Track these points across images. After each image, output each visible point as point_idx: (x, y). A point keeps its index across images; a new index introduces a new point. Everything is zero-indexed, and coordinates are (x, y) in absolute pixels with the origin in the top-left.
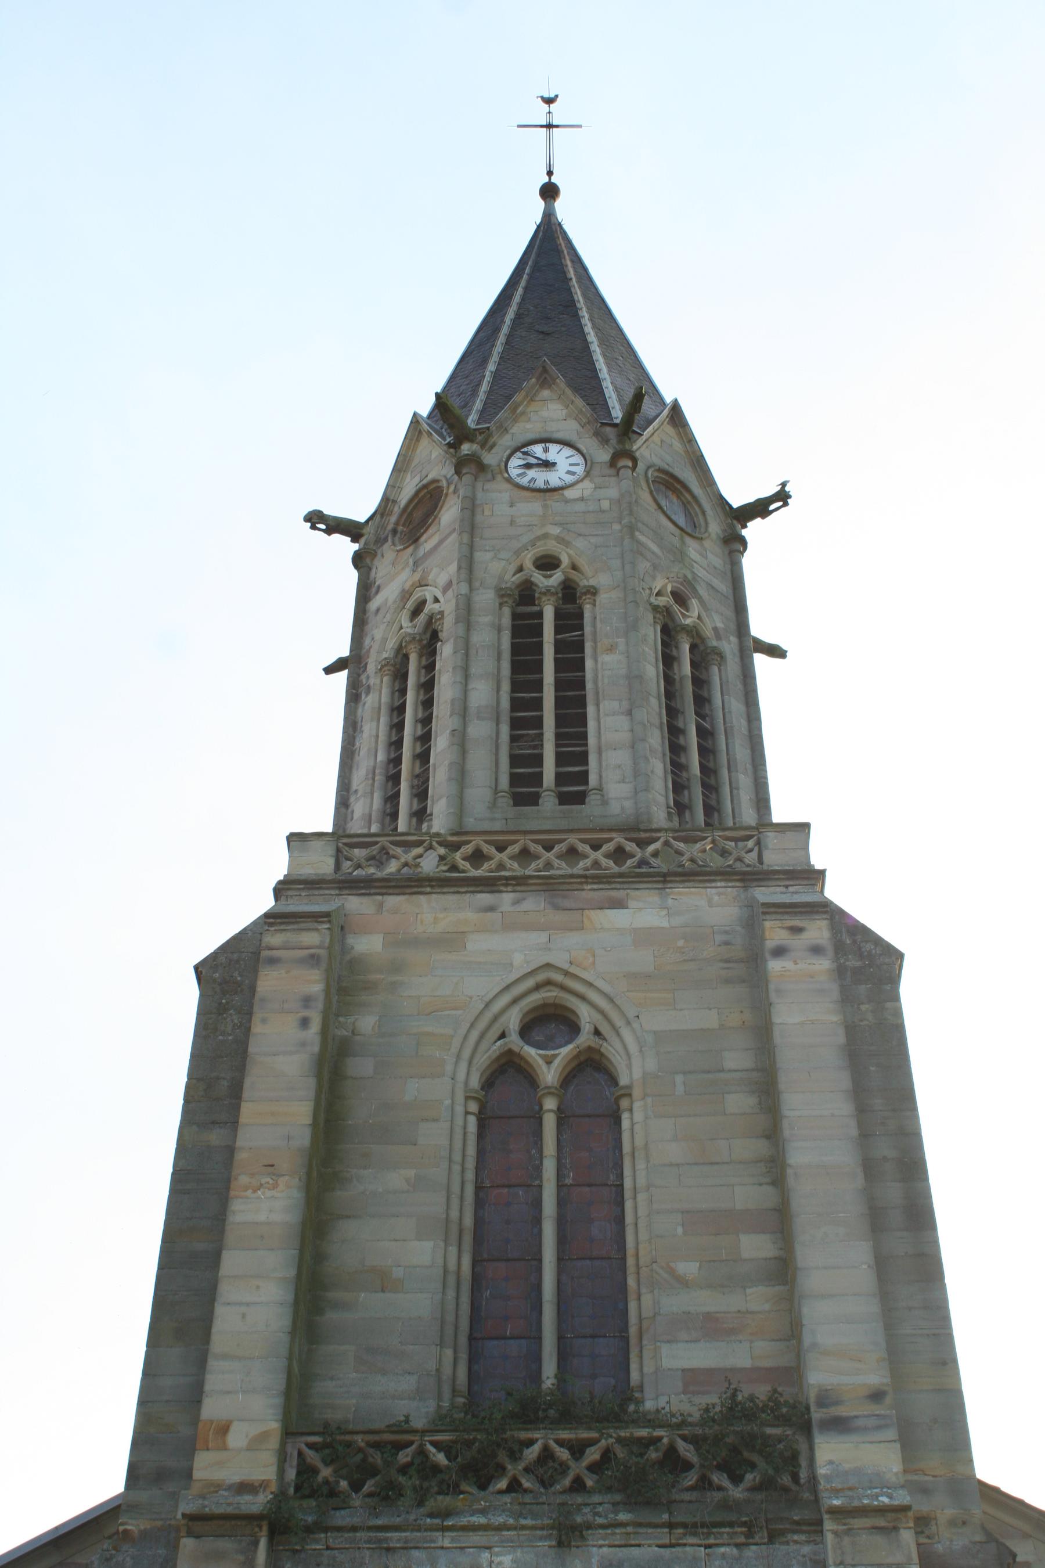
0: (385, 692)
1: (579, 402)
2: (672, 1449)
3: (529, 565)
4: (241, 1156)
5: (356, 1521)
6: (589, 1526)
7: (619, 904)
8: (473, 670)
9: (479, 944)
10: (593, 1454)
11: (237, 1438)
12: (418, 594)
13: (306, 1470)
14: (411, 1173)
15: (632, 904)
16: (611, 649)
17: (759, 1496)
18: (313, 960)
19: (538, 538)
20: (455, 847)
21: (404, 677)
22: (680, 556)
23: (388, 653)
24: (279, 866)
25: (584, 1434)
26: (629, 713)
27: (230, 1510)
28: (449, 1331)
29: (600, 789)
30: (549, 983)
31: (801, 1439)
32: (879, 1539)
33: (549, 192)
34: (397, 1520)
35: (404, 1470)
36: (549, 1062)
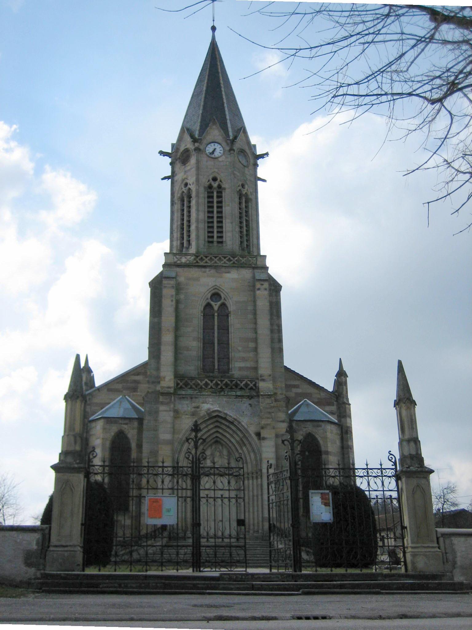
0: (179, 205)
7: (229, 272)
11: (167, 379)
16: (228, 205)
20: (197, 257)
21: (184, 201)
30: (216, 288)
33: (214, 29)
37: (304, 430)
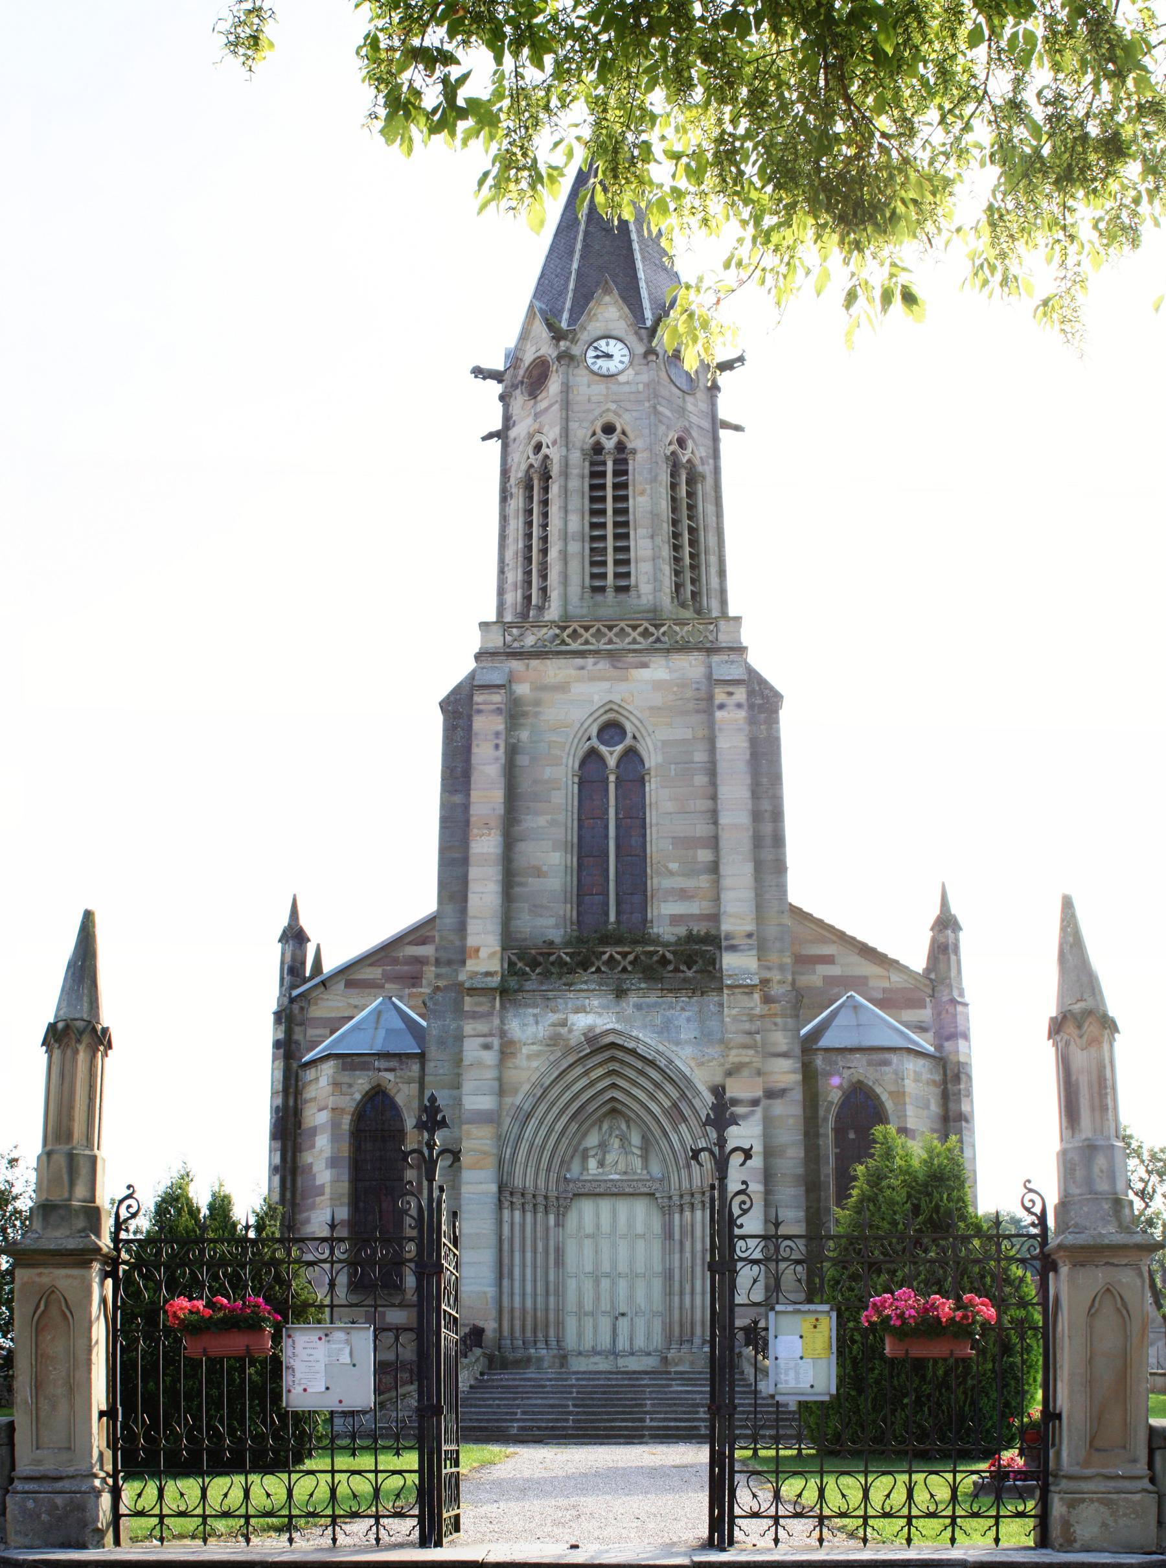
0: (521, 499)
1: (626, 310)
2: (664, 956)
3: (599, 431)
4: (473, 819)
5: (534, 987)
6: (629, 990)
7: (645, 665)
8: (570, 507)
9: (579, 689)
10: (631, 957)
11: (483, 953)
12: (538, 438)
13: (511, 964)
14: (549, 817)
15: (652, 665)
16: (642, 493)
17: (699, 976)
18: (499, 711)
19: (604, 412)
20: (563, 629)
22: (682, 411)
23: (521, 474)
24: (474, 642)
25: (627, 949)
26: (652, 537)
27: (483, 986)
28: (569, 895)
29: (637, 586)
30: (611, 709)
31: (717, 952)
32: (745, 997)
34: (551, 987)
35: (553, 964)
36: (611, 753)
37: (846, 1073)
